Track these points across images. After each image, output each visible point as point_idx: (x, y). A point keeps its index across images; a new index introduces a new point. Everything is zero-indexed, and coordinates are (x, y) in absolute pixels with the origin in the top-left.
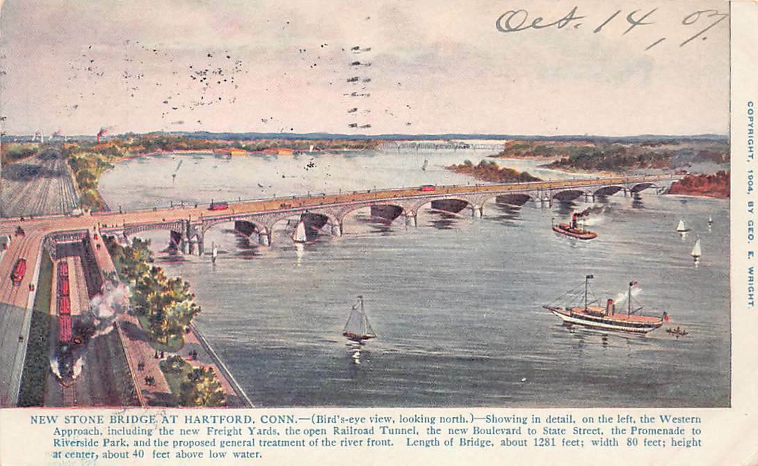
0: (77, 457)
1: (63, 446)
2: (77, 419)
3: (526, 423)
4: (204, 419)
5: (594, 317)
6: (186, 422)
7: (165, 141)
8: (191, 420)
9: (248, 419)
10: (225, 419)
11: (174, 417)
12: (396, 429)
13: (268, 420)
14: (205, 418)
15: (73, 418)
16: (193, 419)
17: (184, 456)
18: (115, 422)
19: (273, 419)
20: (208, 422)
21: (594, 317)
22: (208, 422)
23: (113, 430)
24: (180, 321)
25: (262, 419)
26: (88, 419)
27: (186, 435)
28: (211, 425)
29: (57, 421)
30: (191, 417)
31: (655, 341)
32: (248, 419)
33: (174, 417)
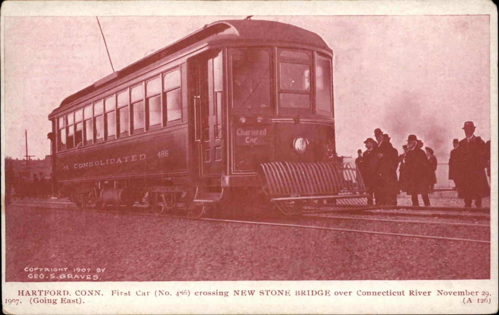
0: (459, 295)
1: (416, 295)
2: (269, 293)
3: (56, 303)
4: (33, 293)
5: (289, 122)
6: (19, 295)
7: (334, 225)
8: (22, 293)
9: (66, 293)
10: (49, 293)
11: (267, 291)
12: (401, 295)
13: (362, 294)
14: (34, 292)
15: (39, 292)
16: (24, 294)
17: (468, 293)
18: (225, 293)
19: (84, 293)
20: (36, 295)
21: (289, 122)
22: (36, 295)
23: (48, 300)
24: (76, 232)
25: (76, 293)
26: (277, 292)
27: (392, 296)
28: (63, 297)
29: (254, 295)
30: (23, 291)
31: (460, 219)
32: (66, 293)
33: (267, 291)
